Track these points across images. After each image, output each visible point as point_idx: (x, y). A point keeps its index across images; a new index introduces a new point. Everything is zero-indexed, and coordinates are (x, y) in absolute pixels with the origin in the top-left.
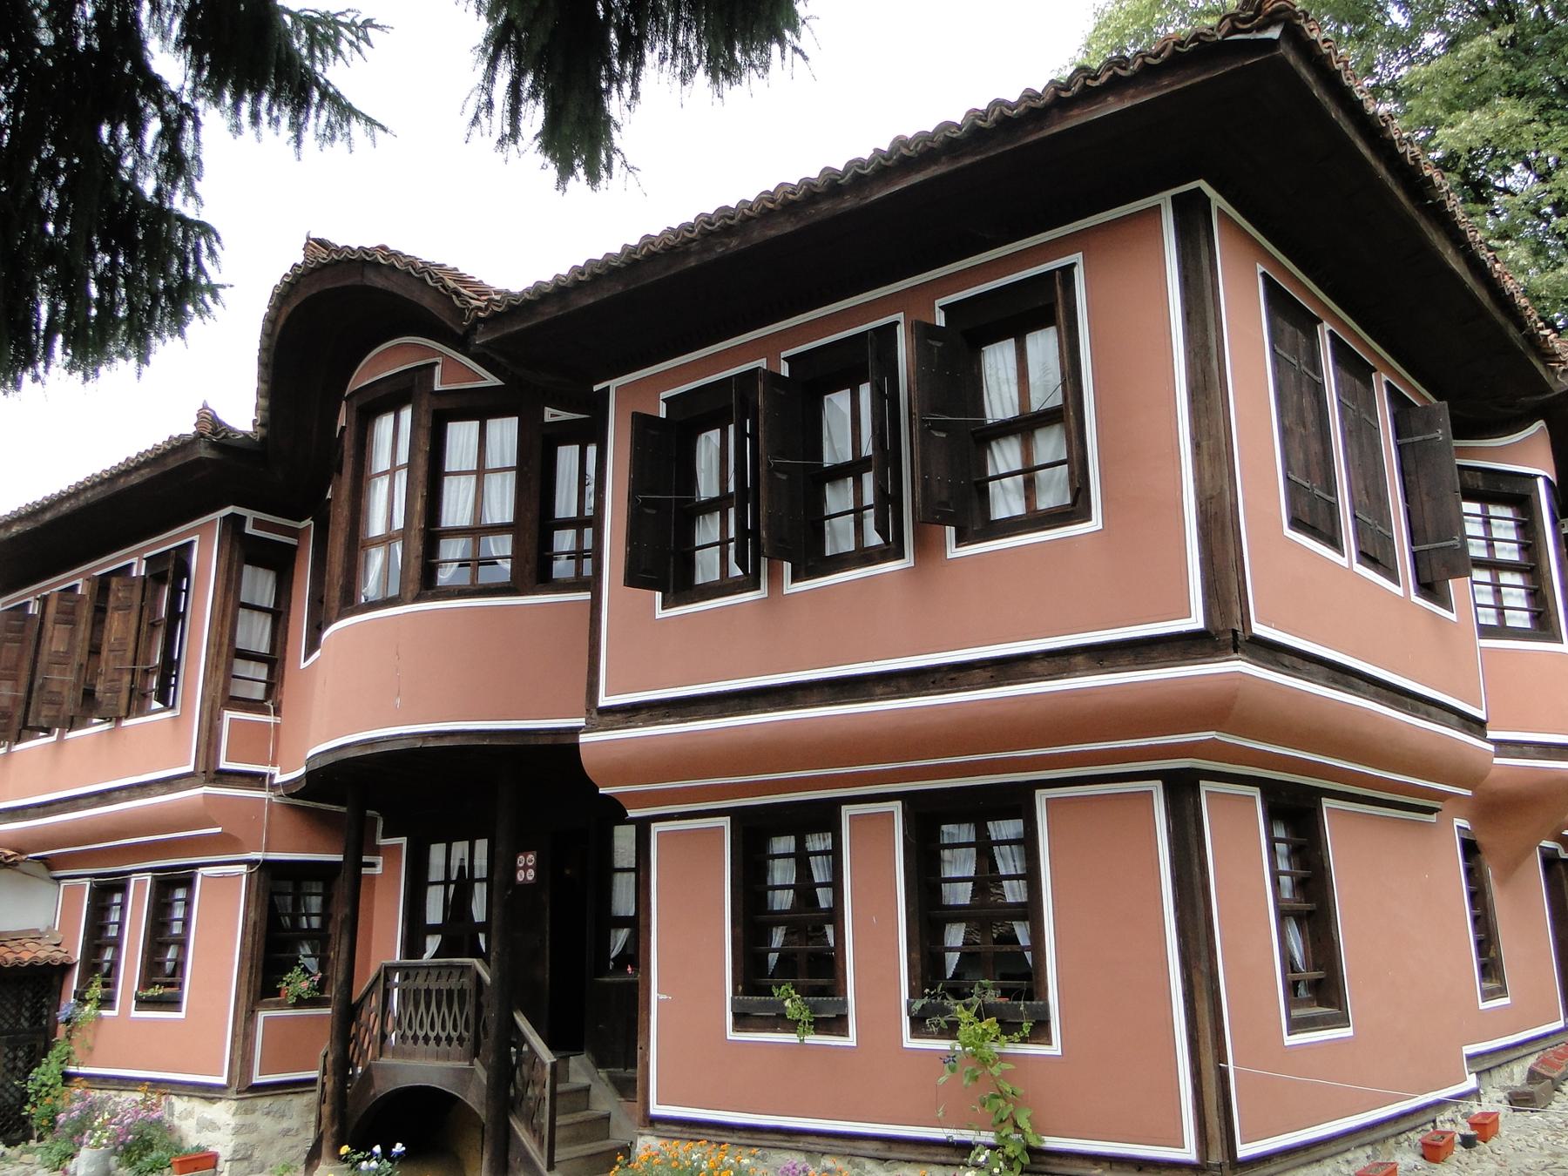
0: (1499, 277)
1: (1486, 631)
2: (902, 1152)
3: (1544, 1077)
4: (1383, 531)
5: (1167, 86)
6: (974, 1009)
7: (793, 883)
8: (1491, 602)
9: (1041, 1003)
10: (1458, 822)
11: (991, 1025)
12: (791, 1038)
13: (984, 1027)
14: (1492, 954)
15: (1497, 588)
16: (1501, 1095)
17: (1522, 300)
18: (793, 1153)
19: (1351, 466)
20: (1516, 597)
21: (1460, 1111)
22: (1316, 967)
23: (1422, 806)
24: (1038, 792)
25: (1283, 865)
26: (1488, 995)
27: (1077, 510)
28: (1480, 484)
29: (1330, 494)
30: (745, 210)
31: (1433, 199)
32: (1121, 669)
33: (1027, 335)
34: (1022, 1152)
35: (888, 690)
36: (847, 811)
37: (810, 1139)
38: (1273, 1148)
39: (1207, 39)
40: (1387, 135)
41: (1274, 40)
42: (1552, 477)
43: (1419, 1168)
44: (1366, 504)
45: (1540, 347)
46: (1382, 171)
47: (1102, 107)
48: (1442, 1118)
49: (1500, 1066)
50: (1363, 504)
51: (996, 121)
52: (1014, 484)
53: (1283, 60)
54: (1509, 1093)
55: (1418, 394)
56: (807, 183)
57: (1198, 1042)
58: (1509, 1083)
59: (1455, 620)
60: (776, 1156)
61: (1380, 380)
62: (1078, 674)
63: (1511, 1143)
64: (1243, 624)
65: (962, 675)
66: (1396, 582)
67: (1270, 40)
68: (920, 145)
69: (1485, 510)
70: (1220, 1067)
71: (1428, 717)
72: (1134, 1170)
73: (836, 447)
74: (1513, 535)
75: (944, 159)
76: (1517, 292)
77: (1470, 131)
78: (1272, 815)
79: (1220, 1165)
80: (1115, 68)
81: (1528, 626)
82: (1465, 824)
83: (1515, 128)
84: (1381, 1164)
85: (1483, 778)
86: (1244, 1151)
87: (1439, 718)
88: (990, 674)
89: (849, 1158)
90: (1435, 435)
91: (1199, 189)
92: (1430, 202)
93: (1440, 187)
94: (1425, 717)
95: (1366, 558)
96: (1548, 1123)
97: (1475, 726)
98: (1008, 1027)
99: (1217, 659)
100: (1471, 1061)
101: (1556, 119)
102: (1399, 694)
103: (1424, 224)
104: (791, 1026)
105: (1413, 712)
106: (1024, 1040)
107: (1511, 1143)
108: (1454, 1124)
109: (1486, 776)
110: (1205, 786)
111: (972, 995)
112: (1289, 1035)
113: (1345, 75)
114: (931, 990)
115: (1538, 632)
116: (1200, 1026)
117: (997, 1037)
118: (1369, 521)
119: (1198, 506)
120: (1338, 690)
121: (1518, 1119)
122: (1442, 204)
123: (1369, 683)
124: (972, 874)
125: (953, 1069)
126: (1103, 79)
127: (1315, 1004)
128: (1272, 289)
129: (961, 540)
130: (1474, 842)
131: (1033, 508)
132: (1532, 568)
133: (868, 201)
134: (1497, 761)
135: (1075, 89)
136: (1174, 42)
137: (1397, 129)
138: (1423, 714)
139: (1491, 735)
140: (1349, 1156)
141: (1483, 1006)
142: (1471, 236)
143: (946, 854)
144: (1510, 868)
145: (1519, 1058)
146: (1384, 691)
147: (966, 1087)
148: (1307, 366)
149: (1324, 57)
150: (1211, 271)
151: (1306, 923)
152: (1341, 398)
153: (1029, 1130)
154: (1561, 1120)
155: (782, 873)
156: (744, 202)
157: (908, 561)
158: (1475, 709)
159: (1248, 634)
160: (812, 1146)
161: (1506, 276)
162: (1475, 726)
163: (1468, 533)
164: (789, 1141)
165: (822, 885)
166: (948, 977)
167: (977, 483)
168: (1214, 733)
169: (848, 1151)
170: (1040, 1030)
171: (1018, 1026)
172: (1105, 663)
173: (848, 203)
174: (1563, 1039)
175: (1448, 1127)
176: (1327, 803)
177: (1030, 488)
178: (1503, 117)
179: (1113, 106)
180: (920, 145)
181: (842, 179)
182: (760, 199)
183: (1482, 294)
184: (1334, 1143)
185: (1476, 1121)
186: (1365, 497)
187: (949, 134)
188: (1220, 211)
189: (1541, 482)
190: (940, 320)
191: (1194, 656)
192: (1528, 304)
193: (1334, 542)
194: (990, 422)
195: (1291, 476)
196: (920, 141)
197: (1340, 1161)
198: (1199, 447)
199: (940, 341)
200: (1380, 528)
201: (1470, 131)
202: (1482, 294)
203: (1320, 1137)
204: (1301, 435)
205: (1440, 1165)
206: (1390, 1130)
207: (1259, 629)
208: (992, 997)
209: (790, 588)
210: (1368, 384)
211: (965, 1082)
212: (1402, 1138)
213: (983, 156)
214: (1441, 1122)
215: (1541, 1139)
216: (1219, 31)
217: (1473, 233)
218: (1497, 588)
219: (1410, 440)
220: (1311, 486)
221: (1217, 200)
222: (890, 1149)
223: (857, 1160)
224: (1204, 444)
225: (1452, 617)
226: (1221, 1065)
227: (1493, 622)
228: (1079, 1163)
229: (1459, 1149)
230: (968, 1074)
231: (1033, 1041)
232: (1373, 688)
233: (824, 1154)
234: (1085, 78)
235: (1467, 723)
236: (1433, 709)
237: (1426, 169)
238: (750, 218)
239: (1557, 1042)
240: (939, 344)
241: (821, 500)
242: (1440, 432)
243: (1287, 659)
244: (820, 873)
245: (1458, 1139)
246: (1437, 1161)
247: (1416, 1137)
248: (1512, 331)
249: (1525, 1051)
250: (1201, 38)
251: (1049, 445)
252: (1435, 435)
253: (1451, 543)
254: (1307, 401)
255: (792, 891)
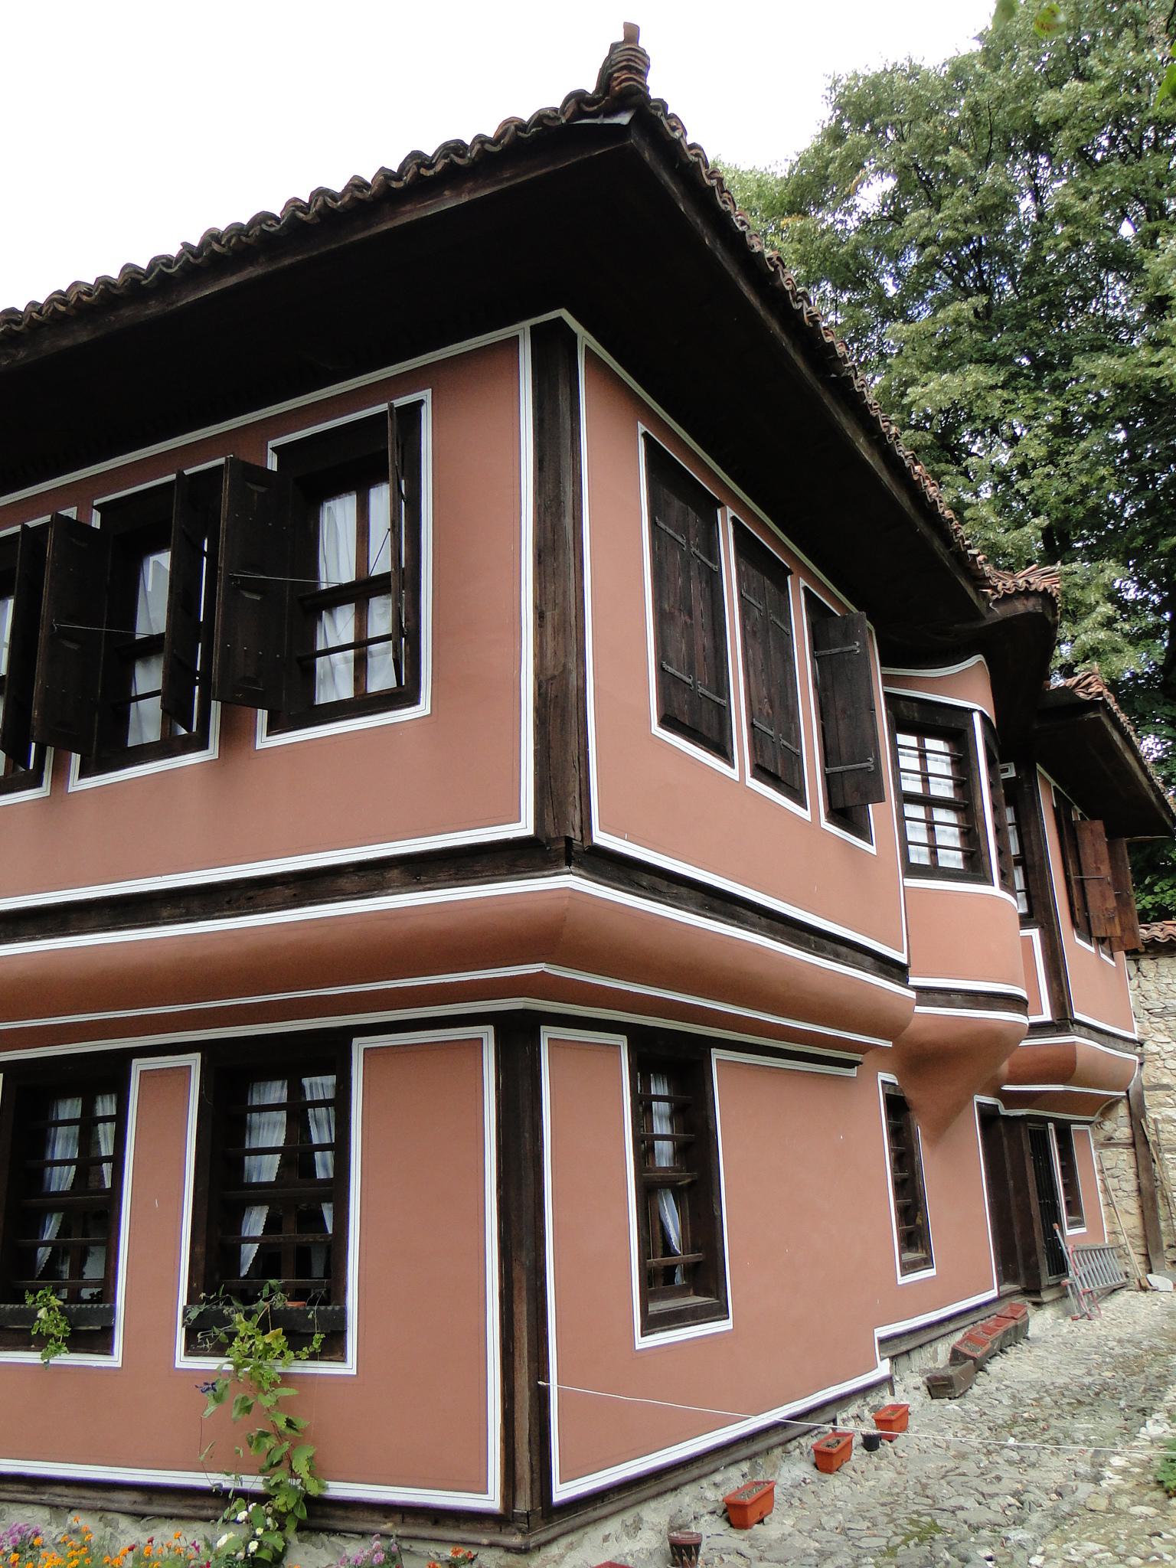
0: (919, 479)
1: (913, 870)
2: (164, 1505)
3: (967, 1357)
4: (789, 746)
5: (508, 179)
6: (257, 1319)
7: (76, 1157)
8: (925, 840)
9: (337, 1308)
10: (883, 1076)
11: (275, 1338)
12: (32, 1357)
13: (267, 1341)
14: (919, 1221)
15: (931, 826)
16: (919, 1380)
17: (946, 512)
18: (36, 1508)
19: (751, 673)
20: (949, 836)
21: (868, 1404)
22: (694, 1249)
23: (845, 1057)
24: (356, 1041)
25: (661, 1127)
26: (908, 1268)
27: (404, 695)
28: (916, 715)
29: (721, 696)
30: (34, 314)
31: (838, 374)
32: (440, 885)
33: (372, 490)
34: (297, 1504)
35: (177, 911)
36: (138, 1065)
37: (58, 1490)
38: (591, 1488)
39: (550, 124)
40: (777, 284)
41: (623, 125)
42: (990, 714)
43: (808, 1481)
44: (768, 714)
45: (969, 568)
46: (775, 327)
47: (435, 203)
48: (844, 1415)
49: (921, 1346)
50: (765, 711)
51: (318, 213)
52: (343, 663)
53: (635, 154)
54: (928, 1379)
55: (838, 603)
56: (105, 282)
57: (513, 1354)
58: (931, 1365)
59: (875, 853)
60: (15, 1512)
61: (796, 590)
62: (390, 891)
63: (918, 1442)
64: (581, 831)
65: (262, 892)
66: (802, 803)
67: (619, 125)
68: (233, 241)
69: (921, 743)
70: (539, 1385)
71: (837, 957)
72: (429, 1523)
73: (151, 616)
74: (948, 771)
75: (262, 259)
76: (941, 502)
77: (938, 391)
78: (642, 1068)
79: (528, 1515)
80: (452, 155)
81: (961, 867)
82: (891, 1078)
83: (981, 392)
84: (758, 1483)
85: (903, 1028)
86: (562, 1492)
87: (849, 959)
88: (293, 892)
89: (100, 1514)
90: (853, 647)
91: (560, 320)
92: (833, 376)
93: (845, 360)
94: (832, 957)
95: (761, 772)
96: (962, 1414)
97: (897, 971)
98: (297, 1340)
99: (546, 873)
100: (883, 1345)
101: (1023, 388)
102: (799, 929)
103: (827, 400)
104: (39, 1342)
105: (818, 951)
106: (313, 1357)
107: (918, 1442)
108: (856, 1423)
109: (909, 1024)
110: (547, 1033)
111: (257, 1299)
112: (643, 1335)
113: (721, 197)
114: (209, 1294)
115: (970, 873)
116: (517, 1334)
117: (282, 1354)
118: (771, 733)
119: (537, 689)
120: (716, 920)
121: (933, 1408)
122: (849, 381)
123: (759, 914)
124: (281, 1144)
125: (218, 1399)
126: (439, 167)
127: (691, 1293)
128: (657, 459)
129: (273, 728)
130: (903, 1098)
131: (362, 692)
132: (967, 806)
133: (174, 307)
134: (919, 1009)
135: (407, 178)
136: (516, 126)
137: (789, 279)
138: (830, 954)
139: (913, 981)
140: (718, 1478)
141: (902, 1280)
142: (885, 427)
143: (255, 1118)
144: (940, 1128)
145: (944, 1335)
146: (781, 925)
147: (235, 1421)
148: (698, 547)
149: (691, 165)
150: (571, 413)
151: (686, 1195)
152: (744, 594)
153: (306, 1476)
154: (977, 1409)
155: (271, 1132)
156: (33, 304)
157: (211, 753)
158: (896, 952)
159: (586, 844)
160: (59, 1499)
161: (928, 481)
162: (897, 971)
163: (901, 767)
164: (33, 1493)
165: (323, 1148)
166: (242, 1275)
167: (300, 660)
168: (543, 965)
169: (99, 1504)
170: (334, 1347)
171: (308, 1339)
172: (422, 878)
173: (153, 308)
174: (992, 1312)
175: (851, 1426)
176: (716, 1054)
177: (361, 665)
178: (969, 379)
179: (449, 201)
180: (233, 241)
181: (146, 278)
182: (51, 300)
183: (905, 501)
184: (696, 1465)
185: (883, 1416)
186: (767, 706)
187: (264, 227)
188: (589, 351)
189: (976, 717)
190: (272, 463)
191: (523, 869)
192: (953, 516)
193: (721, 748)
194: (324, 587)
195: (665, 666)
196: (234, 235)
197: (705, 1486)
198: (543, 617)
199: (263, 486)
200: (786, 743)
201: (938, 391)
202: (905, 501)
203: (660, 1466)
204: (686, 622)
205: (832, 1476)
206: (775, 1439)
207: (601, 838)
208: (280, 1302)
209: (77, 784)
210: (784, 587)
211: (235, 1414)
212: (790, 1446)
213: (306, 256)
214: (844, 1421)
215: (950, 1436)
216: (564, 114)
217: (887, 424)
218: (931, 826)
219: (828, 652)
220: (694, 682)
221: (585, 338)
222: (150, 1502)
223: (110, 1516)
224: (548, 614)
225: (872, 849)
226: (540, 1383)
227: (925, 861)
228: (367, 1515)
229: (858, 1453)
230: (239, 1405)
231: (327, 1358)
232: (764, 921)
233: (71, 1509)
234: (419, 166)
235: (885, 967)
236: (843, 950)
237: (827, 335)
238: (41, 325)
239: (989, 1313)
240: (263, 490)
241: (129, 679)
242: (858, 644)
243: (646, 880)
244: (321, 1133)
245: (858, 1440)
246: (830, 1472)
247: (808, 1442)
248: (937, 544)
249: (952, 1327)
250: (545, 121)
251: (381, 617)
252: (853, 647)
253: (864, 765)
254: (695, 588)
255: (74, 1167)
